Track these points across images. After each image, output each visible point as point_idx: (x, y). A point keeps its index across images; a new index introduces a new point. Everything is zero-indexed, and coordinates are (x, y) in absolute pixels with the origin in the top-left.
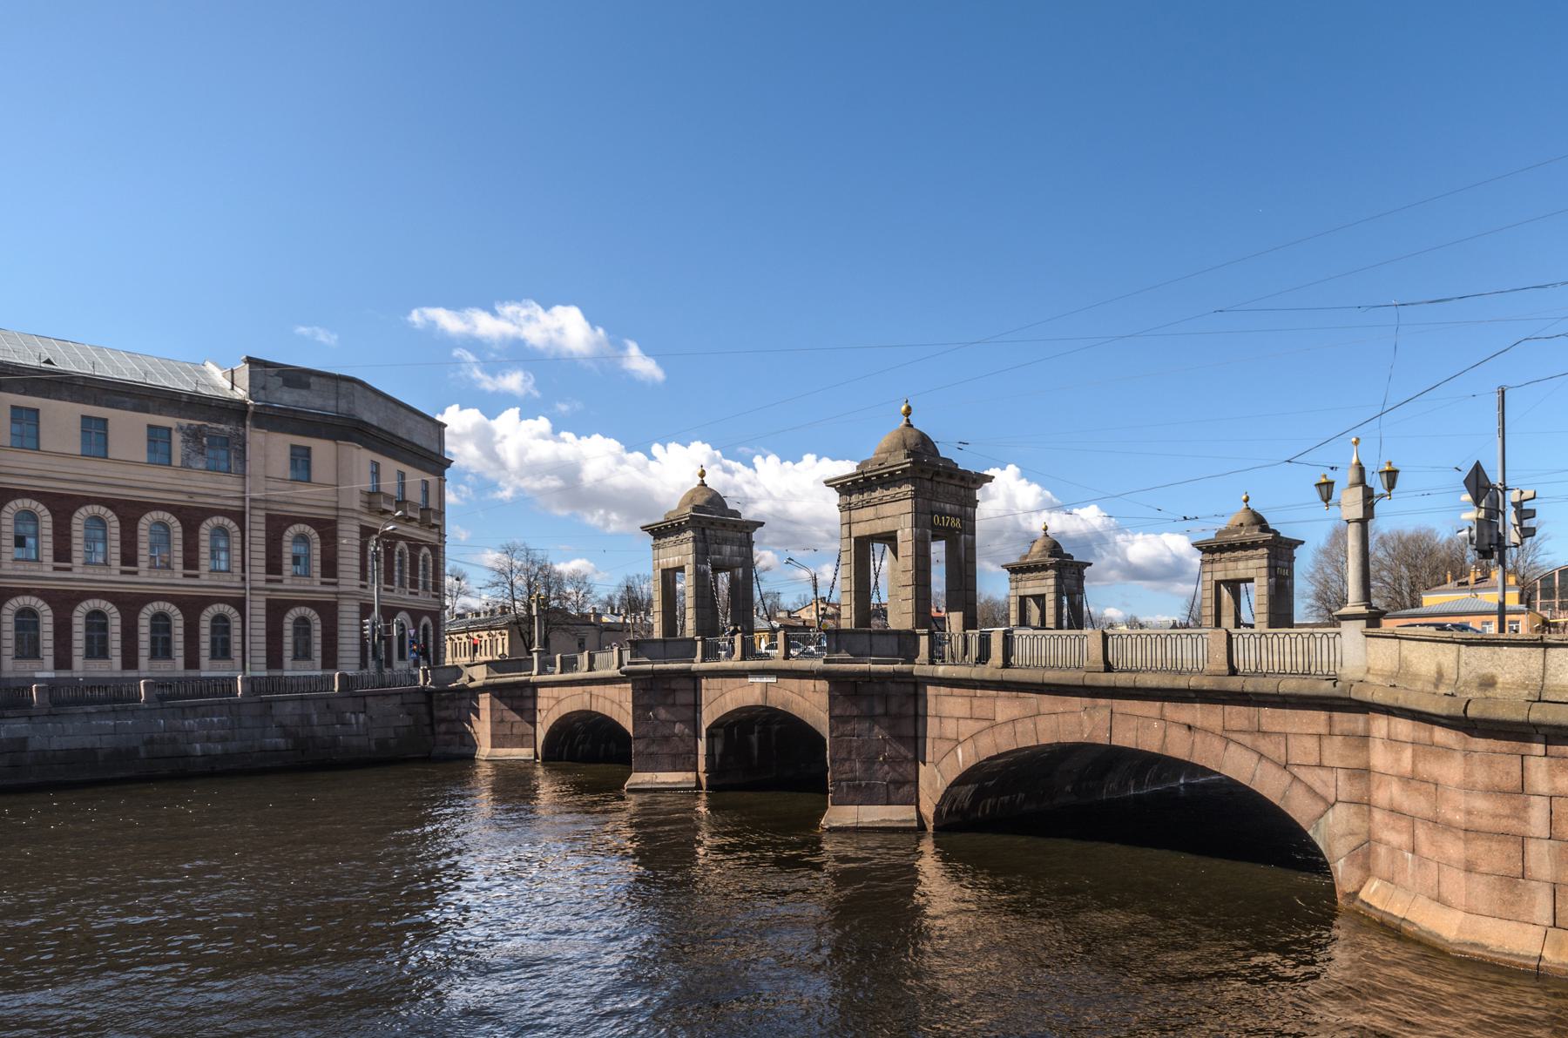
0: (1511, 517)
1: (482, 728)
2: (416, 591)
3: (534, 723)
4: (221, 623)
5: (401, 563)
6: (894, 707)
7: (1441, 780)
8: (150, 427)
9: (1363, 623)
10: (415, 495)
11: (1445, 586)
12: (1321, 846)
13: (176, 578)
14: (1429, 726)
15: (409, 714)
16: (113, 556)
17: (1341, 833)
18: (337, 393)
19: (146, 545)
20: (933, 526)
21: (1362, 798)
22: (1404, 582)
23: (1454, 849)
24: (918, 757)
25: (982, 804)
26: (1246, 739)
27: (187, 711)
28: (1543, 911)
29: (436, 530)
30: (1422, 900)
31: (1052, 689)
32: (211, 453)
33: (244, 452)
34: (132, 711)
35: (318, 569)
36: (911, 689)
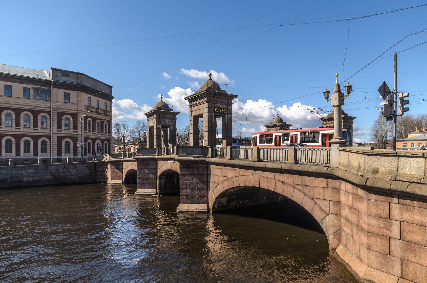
0: (399, 104)
1: (109, 173)
2: (103, 134)
3: (122, 172)
4: (44, 143)
5: (98, 126)
6: (200, 171)
7: (360, 211)
8: (24, 88)
9: (338, 145)
10: (102, 106)
11: (415, 132)
12: (324, 230)
13: (31, 130)
14: (357, 187)
15: (89, 169)
16: (13, 124)
17: (331, 225)
18: (77, 78)
19: (23, 121)
20: (215, 112)
21: (338, 213)
22: (403, 131)
23: (364, 239)
24: (208, 189)
25: (231, 203)
26: (300, 188)
27: (22, 168)
28: (397, 270)
29: (109, 117)
30: (354, 257)
31: (241, 167)
32: (42, 95)
33: (51, 95)
34: (6, 168)
35: (72, 128)
36: (206, 166)
